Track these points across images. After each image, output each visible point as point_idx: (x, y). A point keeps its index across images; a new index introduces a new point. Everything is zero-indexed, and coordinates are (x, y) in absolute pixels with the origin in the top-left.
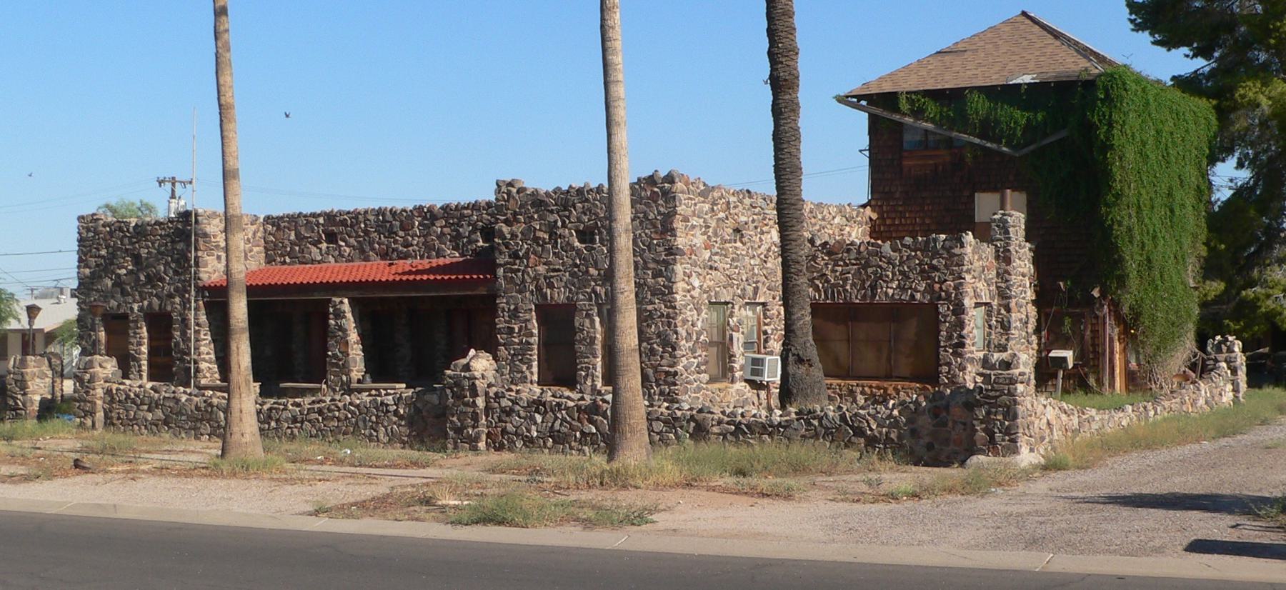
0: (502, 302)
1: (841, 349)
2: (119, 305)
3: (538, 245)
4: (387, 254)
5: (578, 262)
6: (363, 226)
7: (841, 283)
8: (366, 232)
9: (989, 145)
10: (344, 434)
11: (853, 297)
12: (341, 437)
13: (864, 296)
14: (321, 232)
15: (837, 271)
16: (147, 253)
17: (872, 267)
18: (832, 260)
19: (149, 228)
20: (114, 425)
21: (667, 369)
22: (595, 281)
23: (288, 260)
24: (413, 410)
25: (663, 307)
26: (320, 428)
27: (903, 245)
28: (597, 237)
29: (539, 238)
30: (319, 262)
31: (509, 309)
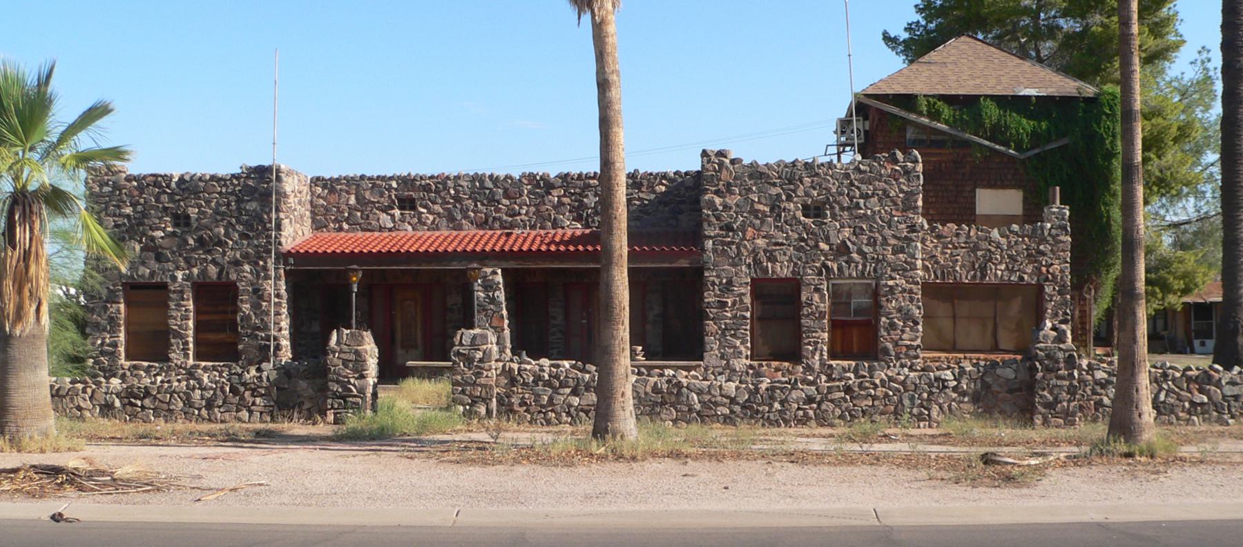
0: (710, 275)
1: (946, 324)
2: (152, 274)
3: (757, 217)
4: (486, 222)
5: (806, 237)
6: (452, 192)
7: (951, 264)
8: (457, 199)
9: (997, 147)
10: (882, 414)
11: (964, 277)
12: (877, 417)
13: (974, 277)
14: (393, 197)
15: (947, 253)
16: (198, 213)
17: (982, 250)
18: (940, 243)
19: (202, 184)
20: (512, 411)
21: (909, 343)
22: (825, 255)
23: (346, 226)
24: (979, 386)
25: (904, 282)
26: (846, 408)
27: (1011, 232)
28: (828, 212)
29: (758, 211)
30: (390, 230)
31: (721, 283)
